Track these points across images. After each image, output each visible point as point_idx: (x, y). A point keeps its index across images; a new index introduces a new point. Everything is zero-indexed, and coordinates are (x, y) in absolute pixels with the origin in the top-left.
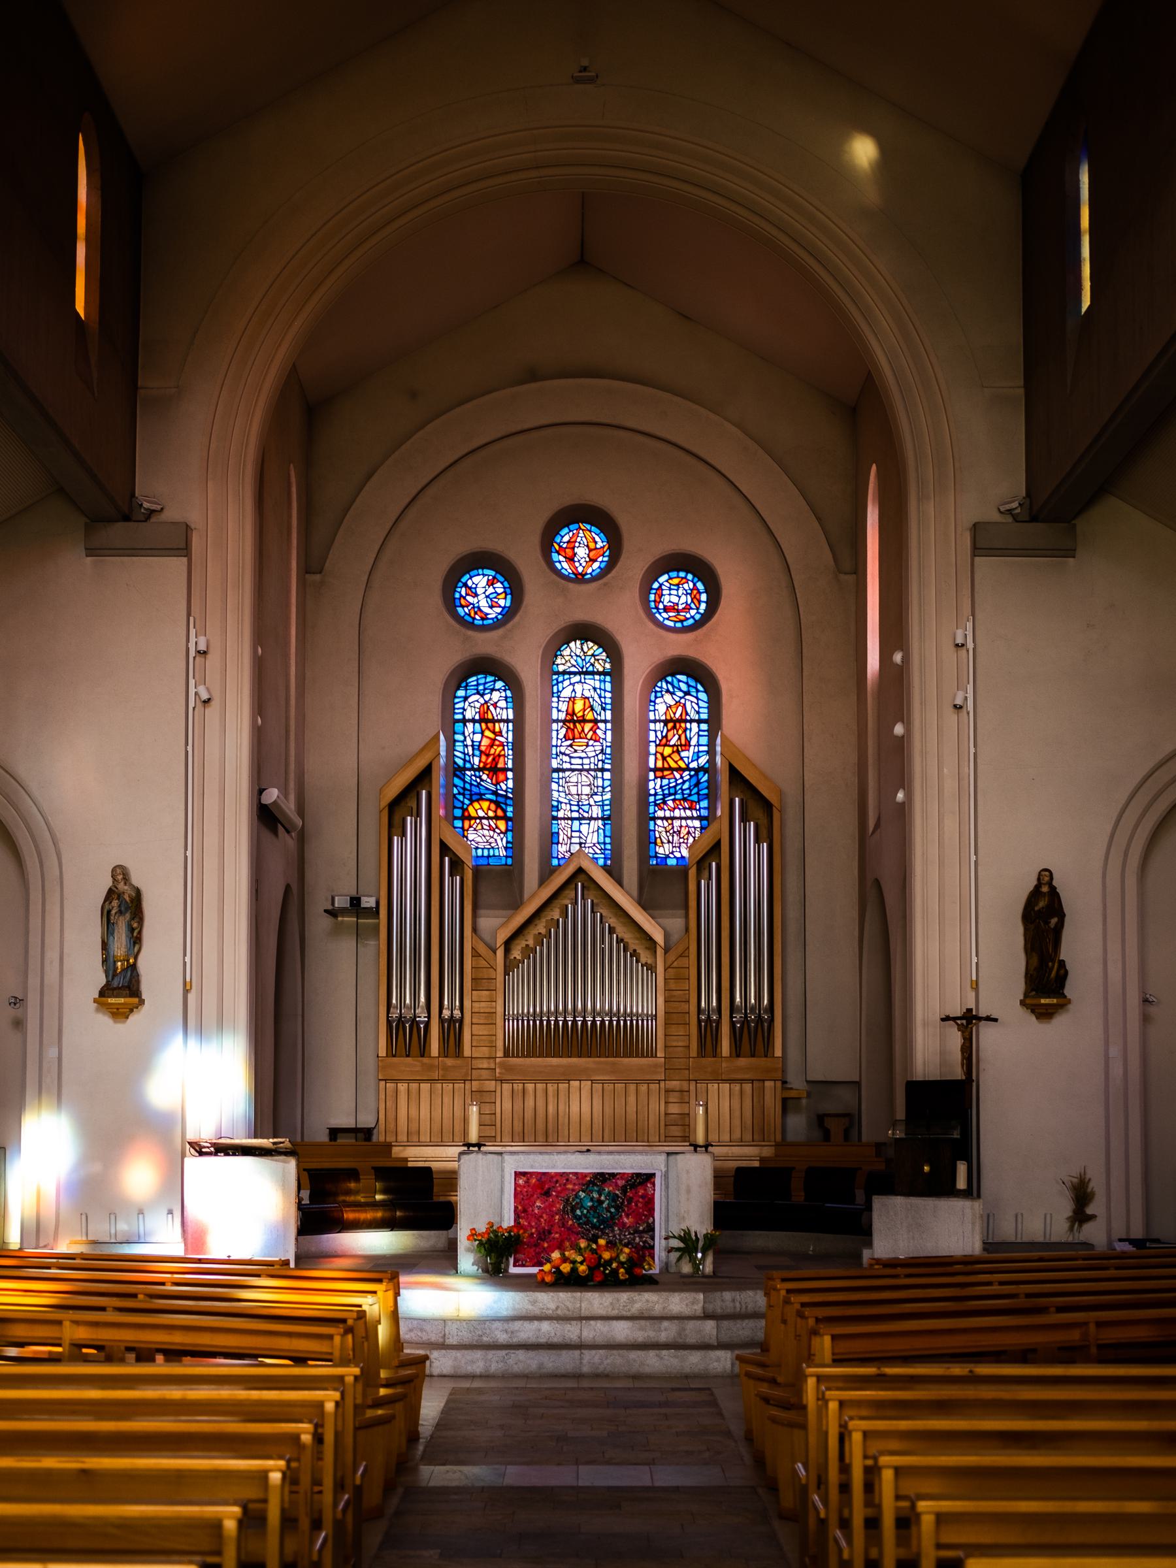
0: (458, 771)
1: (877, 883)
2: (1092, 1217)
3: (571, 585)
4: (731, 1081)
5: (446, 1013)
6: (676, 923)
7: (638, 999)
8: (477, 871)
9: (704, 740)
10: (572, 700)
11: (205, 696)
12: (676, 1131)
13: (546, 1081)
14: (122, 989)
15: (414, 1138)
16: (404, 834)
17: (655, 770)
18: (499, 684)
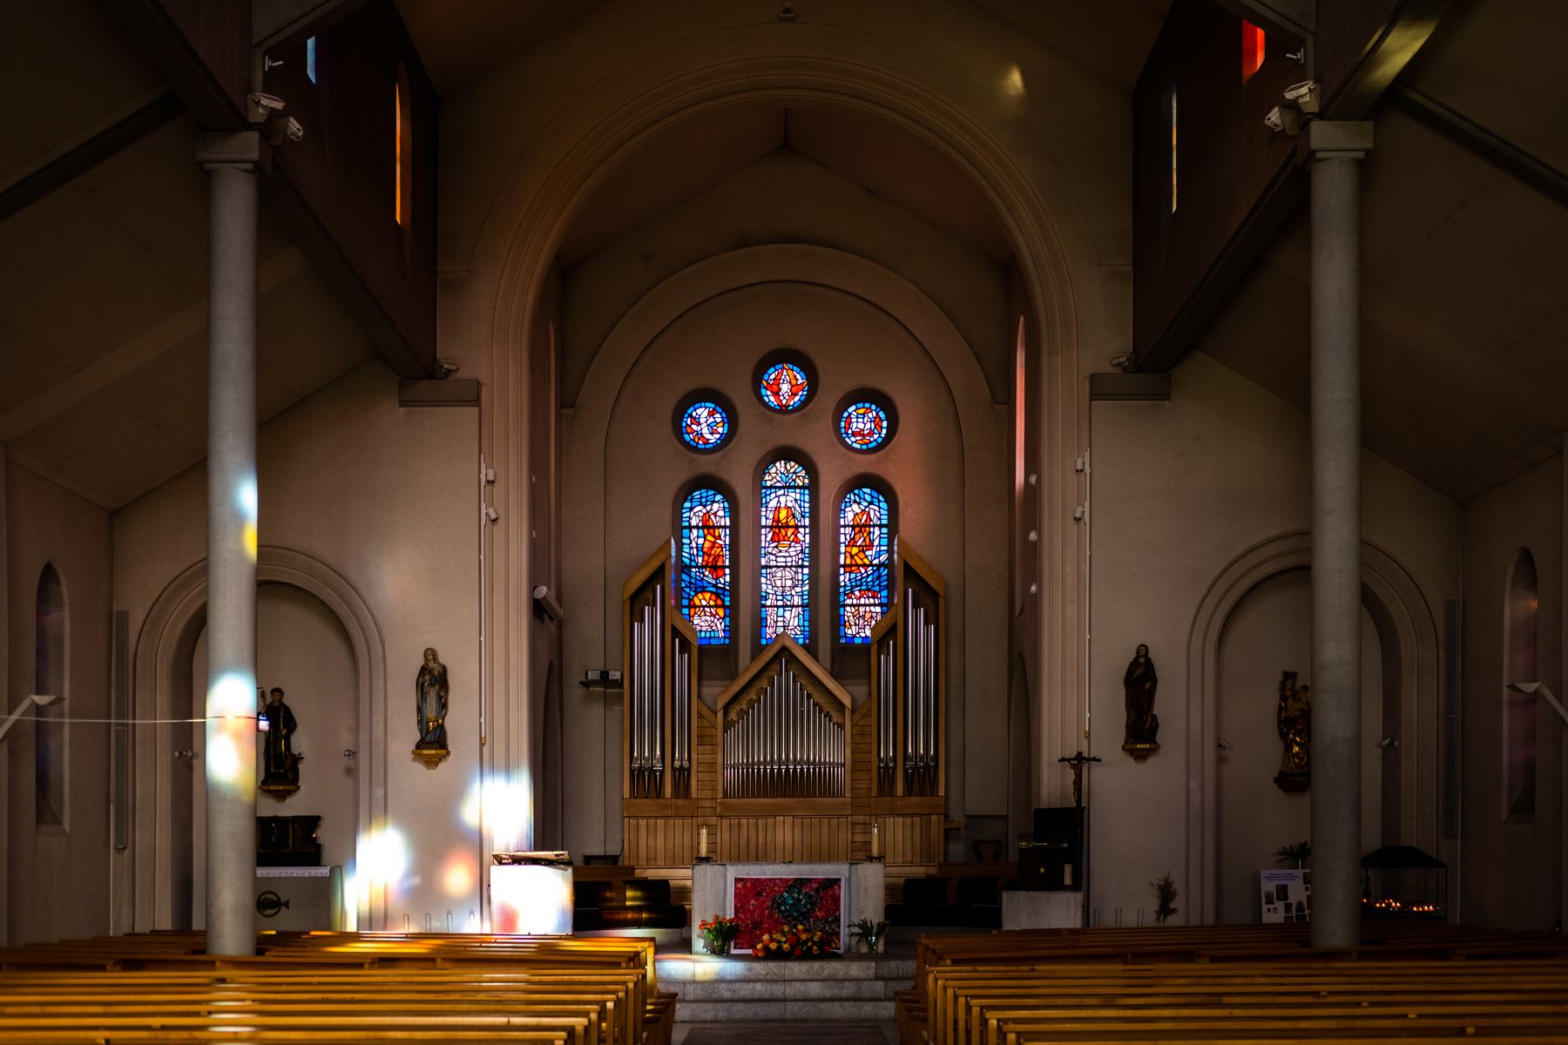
0: (686, 569)
1: (1021, 655)
2: (1175, 911)
3: (777, 415)
4: (904, 815)
5: (677, 764)
6: (861, 690)
7: (829, 751)
8: (701, 648)
9: (884, 541)
10: (778, 509)
11: (493, 516)
12: (860, 855)
13: (756, 817)
14: (433, 743)
15: (651, 862)
16: (642, 620)
17: (845, 566)
18: (719, 497)
